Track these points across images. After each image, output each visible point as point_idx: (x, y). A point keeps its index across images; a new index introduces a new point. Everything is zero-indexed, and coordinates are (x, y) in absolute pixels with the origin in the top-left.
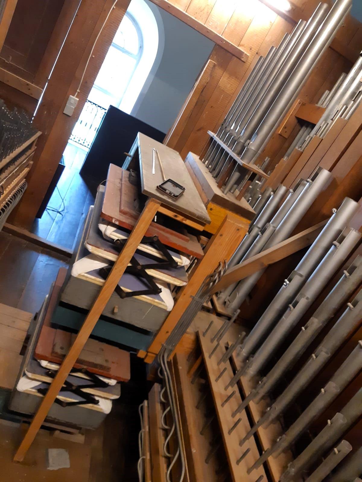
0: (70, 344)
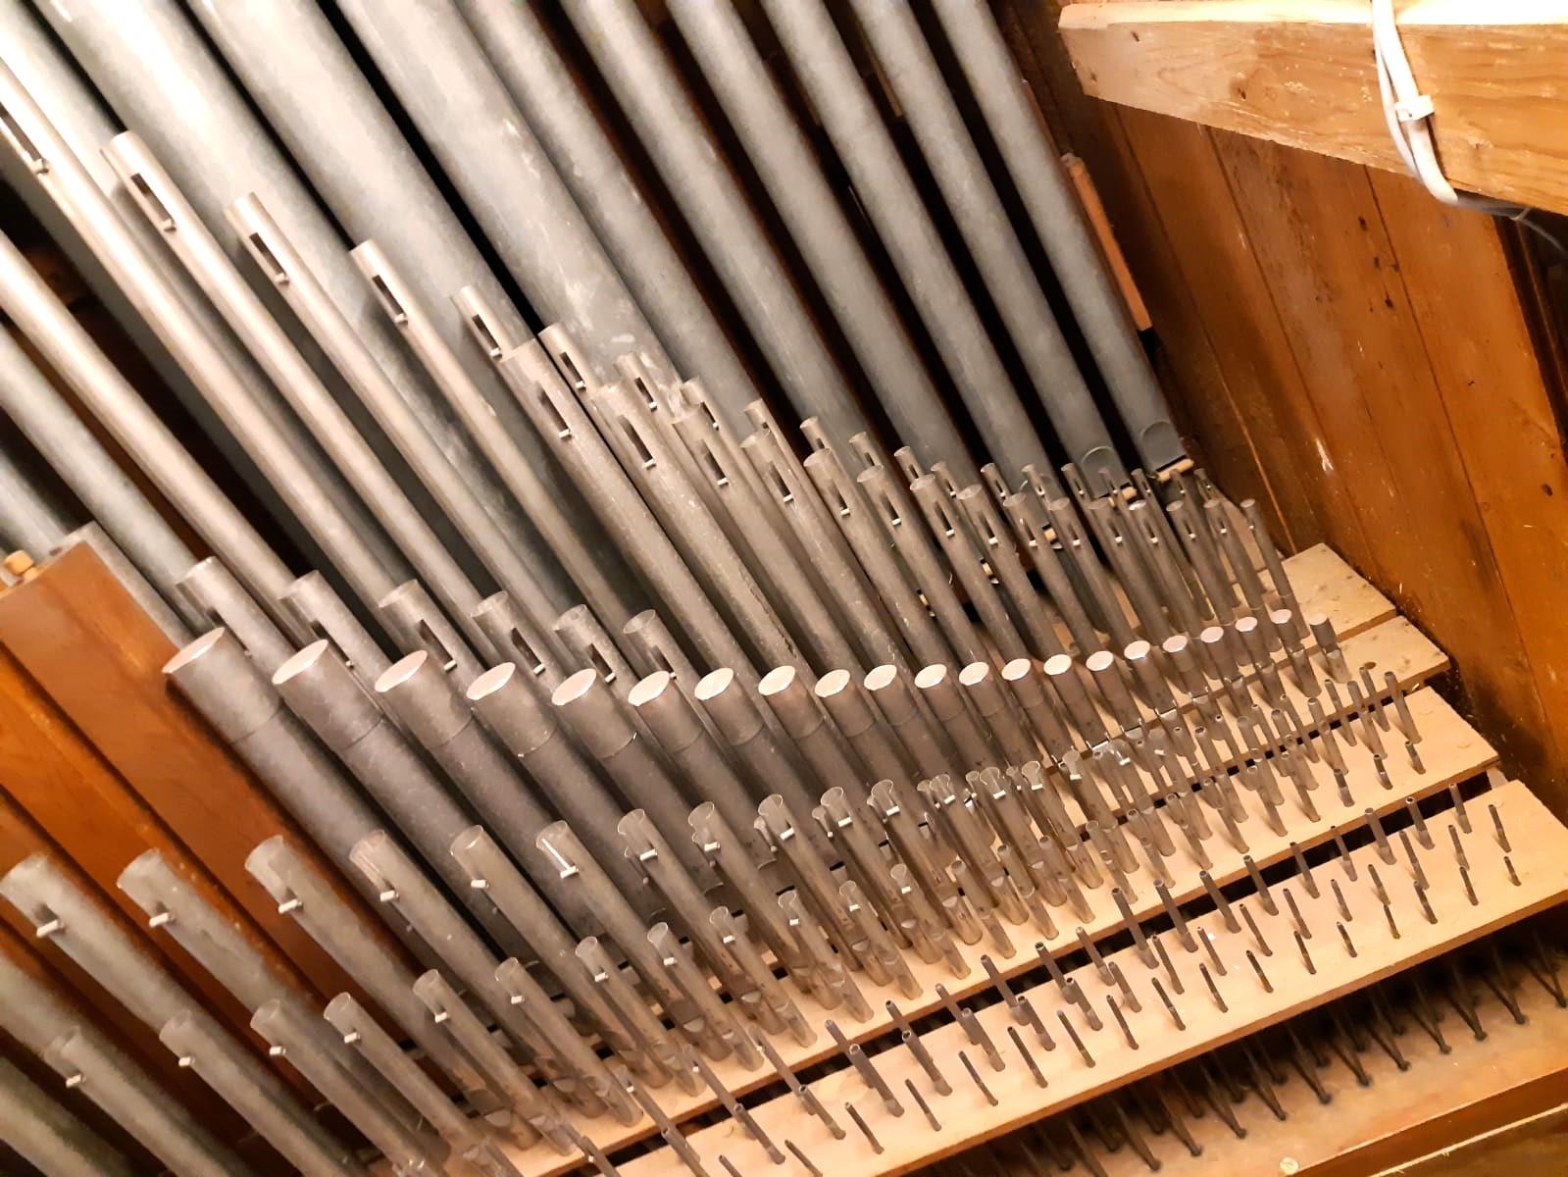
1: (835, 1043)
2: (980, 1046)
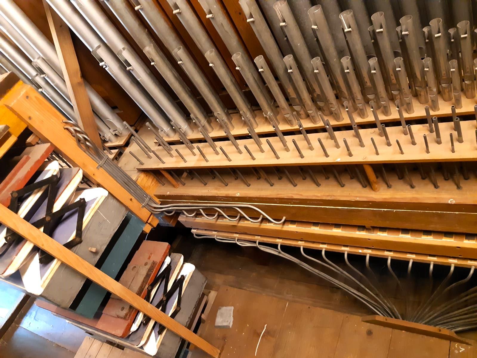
0: (120, 300)
1: (425, 115)
2: (333, 140)
